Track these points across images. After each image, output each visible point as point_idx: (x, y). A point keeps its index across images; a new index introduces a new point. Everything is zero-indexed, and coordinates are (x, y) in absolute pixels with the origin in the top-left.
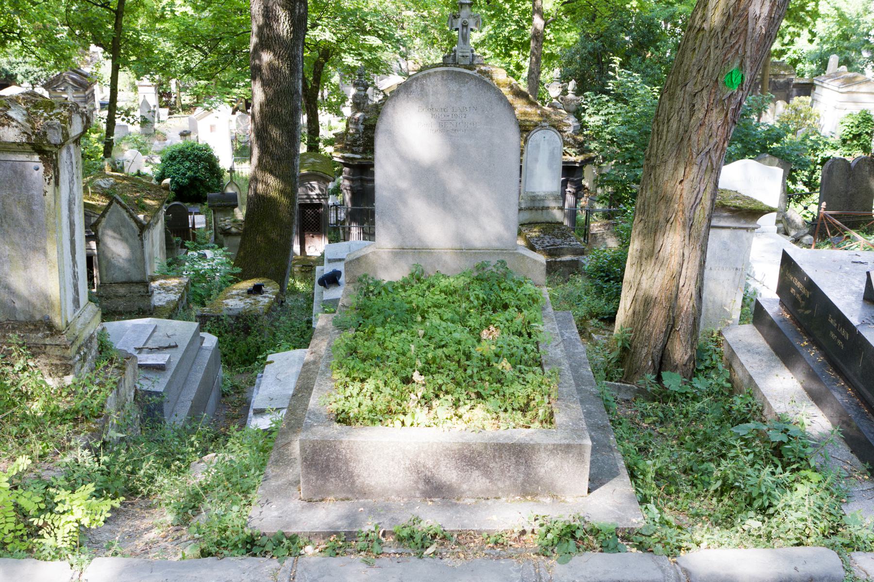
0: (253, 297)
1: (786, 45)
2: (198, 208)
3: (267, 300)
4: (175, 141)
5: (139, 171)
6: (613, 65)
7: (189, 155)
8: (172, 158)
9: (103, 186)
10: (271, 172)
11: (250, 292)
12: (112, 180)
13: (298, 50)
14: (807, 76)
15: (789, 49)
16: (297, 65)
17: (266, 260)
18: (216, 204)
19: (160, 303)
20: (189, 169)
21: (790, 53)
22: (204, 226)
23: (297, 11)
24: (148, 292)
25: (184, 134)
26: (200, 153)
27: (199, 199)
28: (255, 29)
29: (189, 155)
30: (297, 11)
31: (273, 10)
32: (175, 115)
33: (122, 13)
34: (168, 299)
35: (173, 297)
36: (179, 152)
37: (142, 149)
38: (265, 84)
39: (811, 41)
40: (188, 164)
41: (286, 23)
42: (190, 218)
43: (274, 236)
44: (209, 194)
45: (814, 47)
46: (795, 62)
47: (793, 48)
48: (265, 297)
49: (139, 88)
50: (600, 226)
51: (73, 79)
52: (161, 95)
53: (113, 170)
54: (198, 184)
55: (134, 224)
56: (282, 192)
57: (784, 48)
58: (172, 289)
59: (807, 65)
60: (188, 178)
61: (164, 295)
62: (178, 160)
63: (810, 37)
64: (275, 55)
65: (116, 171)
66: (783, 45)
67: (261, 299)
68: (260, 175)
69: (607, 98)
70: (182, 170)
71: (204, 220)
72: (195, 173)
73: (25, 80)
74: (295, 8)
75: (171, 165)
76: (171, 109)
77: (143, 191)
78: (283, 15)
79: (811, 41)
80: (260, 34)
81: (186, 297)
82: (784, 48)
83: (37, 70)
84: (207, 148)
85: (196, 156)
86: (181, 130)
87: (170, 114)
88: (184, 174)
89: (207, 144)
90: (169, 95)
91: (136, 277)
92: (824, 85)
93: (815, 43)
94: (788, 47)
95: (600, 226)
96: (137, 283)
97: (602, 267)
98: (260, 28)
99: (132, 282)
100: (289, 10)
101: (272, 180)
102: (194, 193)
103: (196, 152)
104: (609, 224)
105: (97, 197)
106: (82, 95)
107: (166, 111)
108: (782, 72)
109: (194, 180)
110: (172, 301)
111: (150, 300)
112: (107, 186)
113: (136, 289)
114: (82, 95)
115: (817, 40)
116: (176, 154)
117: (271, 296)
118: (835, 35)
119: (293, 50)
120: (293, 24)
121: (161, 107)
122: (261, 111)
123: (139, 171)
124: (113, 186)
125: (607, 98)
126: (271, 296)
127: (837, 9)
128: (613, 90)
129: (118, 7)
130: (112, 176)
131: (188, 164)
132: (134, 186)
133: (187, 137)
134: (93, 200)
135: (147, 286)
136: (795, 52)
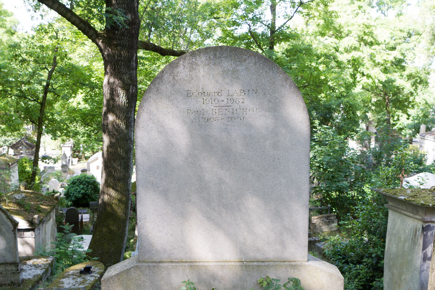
0: (83, 276)
1: (395, 121)
2: (86, 210)
3: (92, 279)
4: (78, 173)
5: (54, 190)
6: (315, 125)
7: (83, 182)
8: (74, 183)
9: (17, 198)
10: (113, 188)
11: (82, 272)
12: (24, 195)
13: (131, 113)
14: (408, 136)
15: (397, 123)
16: (130, 123)
17: (109, 244)
18: (94, 208)
19: (29, 277)
20: (83, 189)
21: (398, 125)
22: (88, 220)
23: (131, 91)
24: (18, 270)
25: (84, 171)
26: (89, 180)
27: (86, 205)
28: (105, 102)
29: (83, 182)
30: (131, 91)
31: (116, 90)
32: (81, 161)
33: (44, 104)
34: (35, 273)
35: (39, 272)
36: (78, 180)
37: (59, 179)
38: (111, 135)
39: (408, 119)
40: (82, 186)
41: (124, 98)
42: (80, 215)
43: (114, 228)
44: (91, 203)
45: (410, 122)
46: (401, 129)
47: (399, 122)
48: (92, 276)
49: (62, 148)
50: (318, 219)
51: (26, 143)
52: (75, 152)
53: (25, 189)
54: (87, 197)
55: (10, 223)
56: (120, 200)
57: (394, 122)
58: (40, 266)
59: (407, 131)
60: (81, 194)
61: (33, 270)
62: (76, 184)
63: (407, 117)
64: (117, 117)
65: (28, 189)
66: (394, 121)
67: (89, 278)
68: (330, 226)
69: (314, 143)
70: (79, 190)
71: (89, 217)
72: (86, 191)
73: (4, 145)
74: (129, 89)
75: (73, 187)
76: (79, 159)
77: (42, 201)
78: (121, 93)
79: (408, 119)
80: (108, 105)
81: (50, 271)
82: (394, 122)
83: (11, 139)
84: (93, 177)
85: (86, 182)
86: (82, 169)
87: (79, 161)
88: (79, 192)
89: (93, 175)
90: (79, 152)
91: (10, 259)
92: (426, 138)
93: (410, 120)
94: (397, 122)
95: (318, 219)
96: (11, 264)
97: (339, 251)
98: (108, 101)
99: (7, 264)
100: (126, 90)
101: (113, 193)
102: (85, 202)
103: (86, 180)
104: (323, 217)
105: (11, 205)
106: (31, 151)
107: (77, 159)
108: (396, 134)
109: (85, 195)
110: (37, 275)
111: (19, 276)
112: (20, 198)
113: (9, 268)
114: (31, 151)
115: (411, 118)
116: (76, 181)
117: (96, 275)
118: (420, 116)
119: (128, 113)
120: (128, 98)
121: (74, 157)
122: (108, 151)
123: (54, 190)
124: (24, 199)
125: (314, 143)
126: (96, 275)
127: (425, 100)
128: (317, 139)
129: (43, 100)
130: (24, 192)
131: (82, 186)
132: (37, 198)
133: (85, 172)
134: (9, 206)
135: (18, 266)
136: (400, 124)
